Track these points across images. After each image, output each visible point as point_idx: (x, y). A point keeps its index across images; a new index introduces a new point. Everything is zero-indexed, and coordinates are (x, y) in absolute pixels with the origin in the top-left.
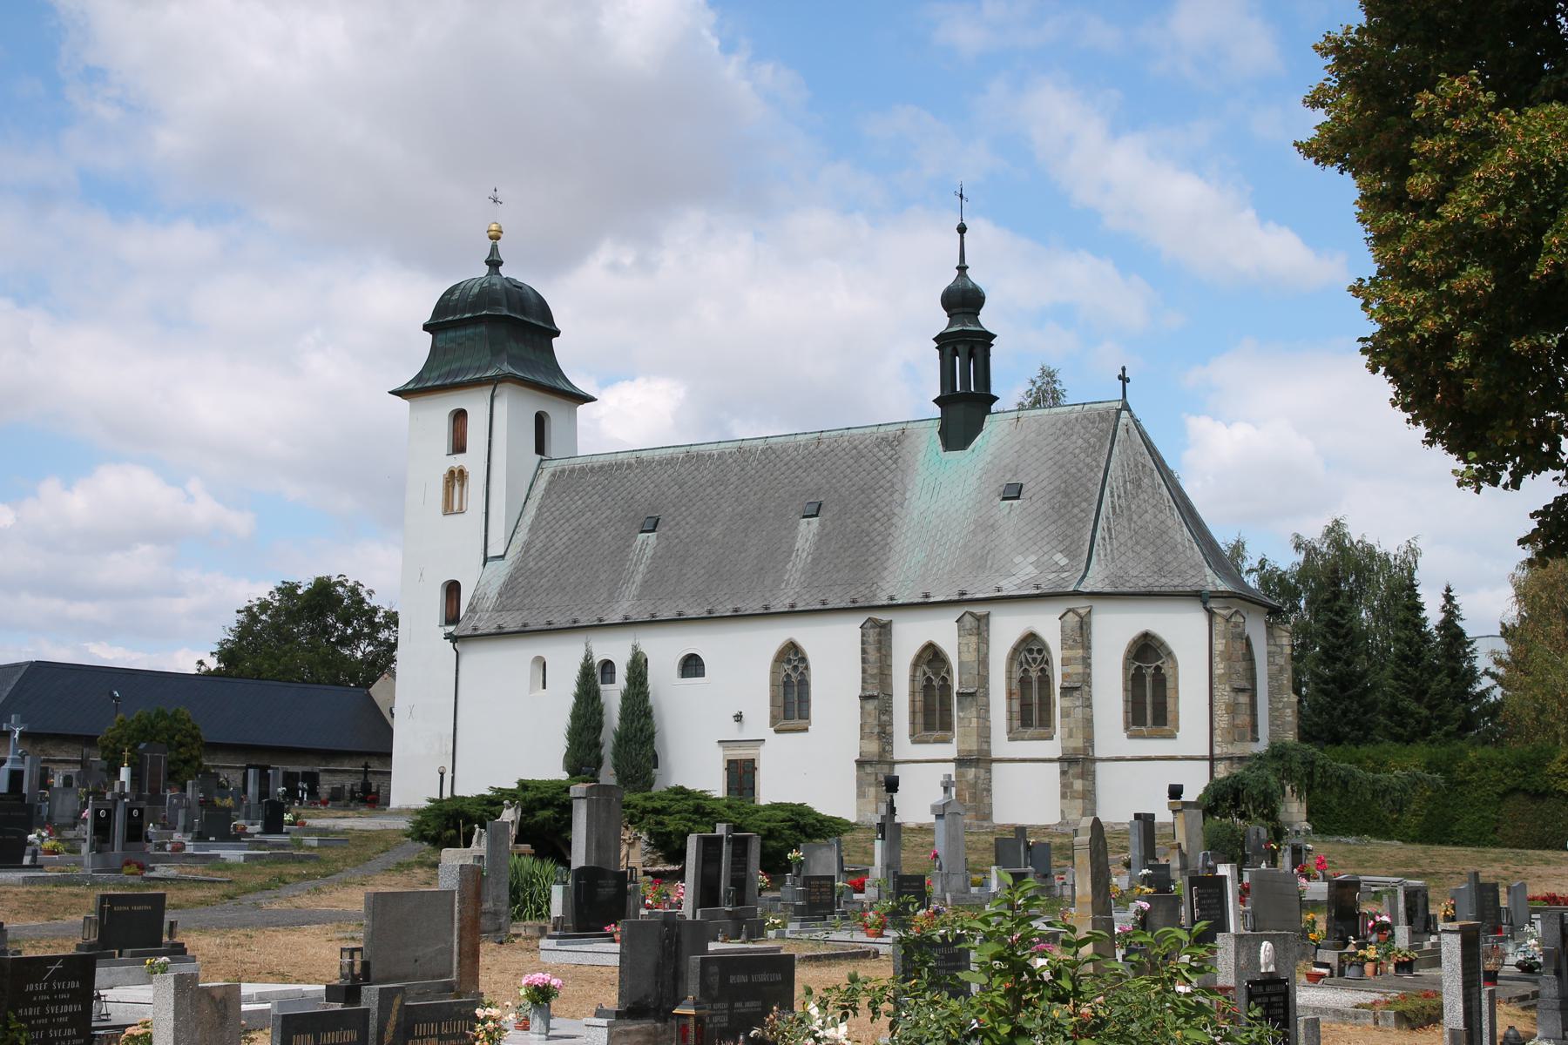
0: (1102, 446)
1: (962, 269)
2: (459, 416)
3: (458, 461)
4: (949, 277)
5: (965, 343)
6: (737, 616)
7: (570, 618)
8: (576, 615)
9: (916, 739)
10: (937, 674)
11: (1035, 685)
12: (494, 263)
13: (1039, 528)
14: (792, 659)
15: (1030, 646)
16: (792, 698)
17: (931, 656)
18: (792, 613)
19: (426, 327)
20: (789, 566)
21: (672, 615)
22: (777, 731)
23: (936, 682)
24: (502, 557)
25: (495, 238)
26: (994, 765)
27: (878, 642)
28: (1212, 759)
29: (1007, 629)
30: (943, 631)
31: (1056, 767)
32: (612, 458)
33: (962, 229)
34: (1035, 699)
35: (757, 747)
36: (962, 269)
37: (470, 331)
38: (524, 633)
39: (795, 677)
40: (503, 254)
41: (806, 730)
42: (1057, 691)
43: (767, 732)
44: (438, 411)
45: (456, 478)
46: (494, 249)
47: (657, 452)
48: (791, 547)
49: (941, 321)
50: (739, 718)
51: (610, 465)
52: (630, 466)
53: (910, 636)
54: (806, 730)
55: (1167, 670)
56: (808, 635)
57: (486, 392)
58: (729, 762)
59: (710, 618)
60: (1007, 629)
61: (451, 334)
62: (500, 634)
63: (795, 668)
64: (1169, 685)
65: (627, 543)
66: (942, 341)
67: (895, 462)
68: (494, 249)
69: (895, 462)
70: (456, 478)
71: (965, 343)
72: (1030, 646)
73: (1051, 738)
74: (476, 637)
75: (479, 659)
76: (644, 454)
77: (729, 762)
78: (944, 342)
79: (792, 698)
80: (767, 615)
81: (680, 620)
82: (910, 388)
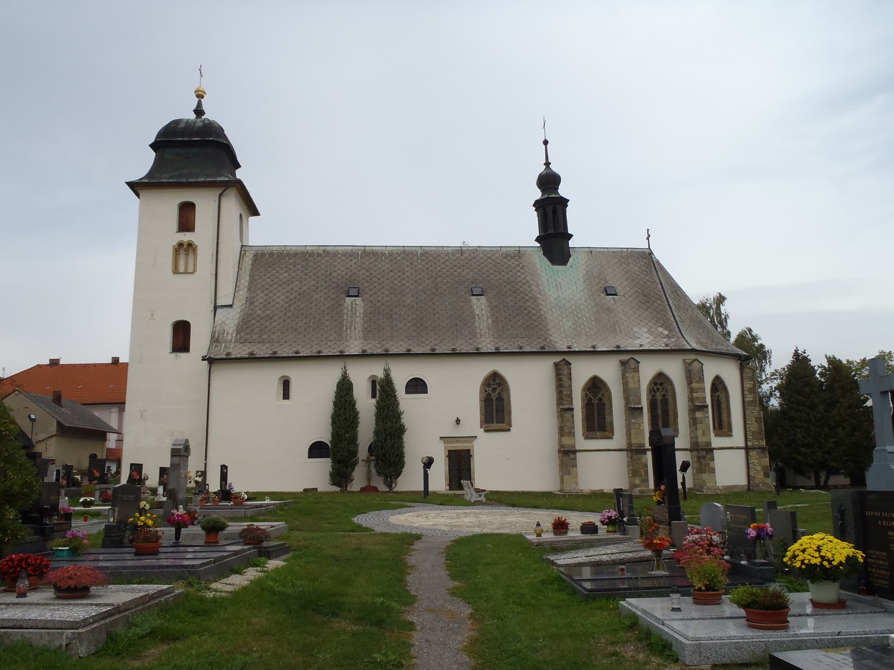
0: (651, 271)
1: (547, 164)
3: (186, 237)
5: (551, 209)
6: (454, 354)
7: (383, 348)
8: (388, 346)
10: (595, 396)
11: (659, 405)
12: (199, 112)
13: (639, 313)
16: (496, 408)
18: (497, 353)
19: (152, 146)
20: (477, 324)
22: (486, 431)
24: (231, 306)
27: (562, 375)
28: (747, 449)
31: (743, 452)
33: (546, 143)
34: (660, 412)
35: (471, 442)
36: (547, 164)
38: (274, 358)
39: (494, 396)
40: (205, 108)
41: (509, 430)
43: (479, 432)
44: (168, 204)
45: (185, 249)
46: (199, 104)
48: (472, 313)
49: (538, 194)
50: (458, 421)
51: (303, 253)
53: (582, 372)
54: (509, 430)
56: (509, 369)
57: (218, 192)
59: (433, 355)
60: (648, 369)
63: (494, 390)
64: (607, 406)
65: (338, 307)
66: (538, 205)
67: (522, 268)
68: (199, 104)
70: (185, 249)
71: (551, 209)
74: (229, 360)
76: (328, 249)
78: (539, 205)
79: (496, 408)
80: (478, 354)
82: (524, 231)
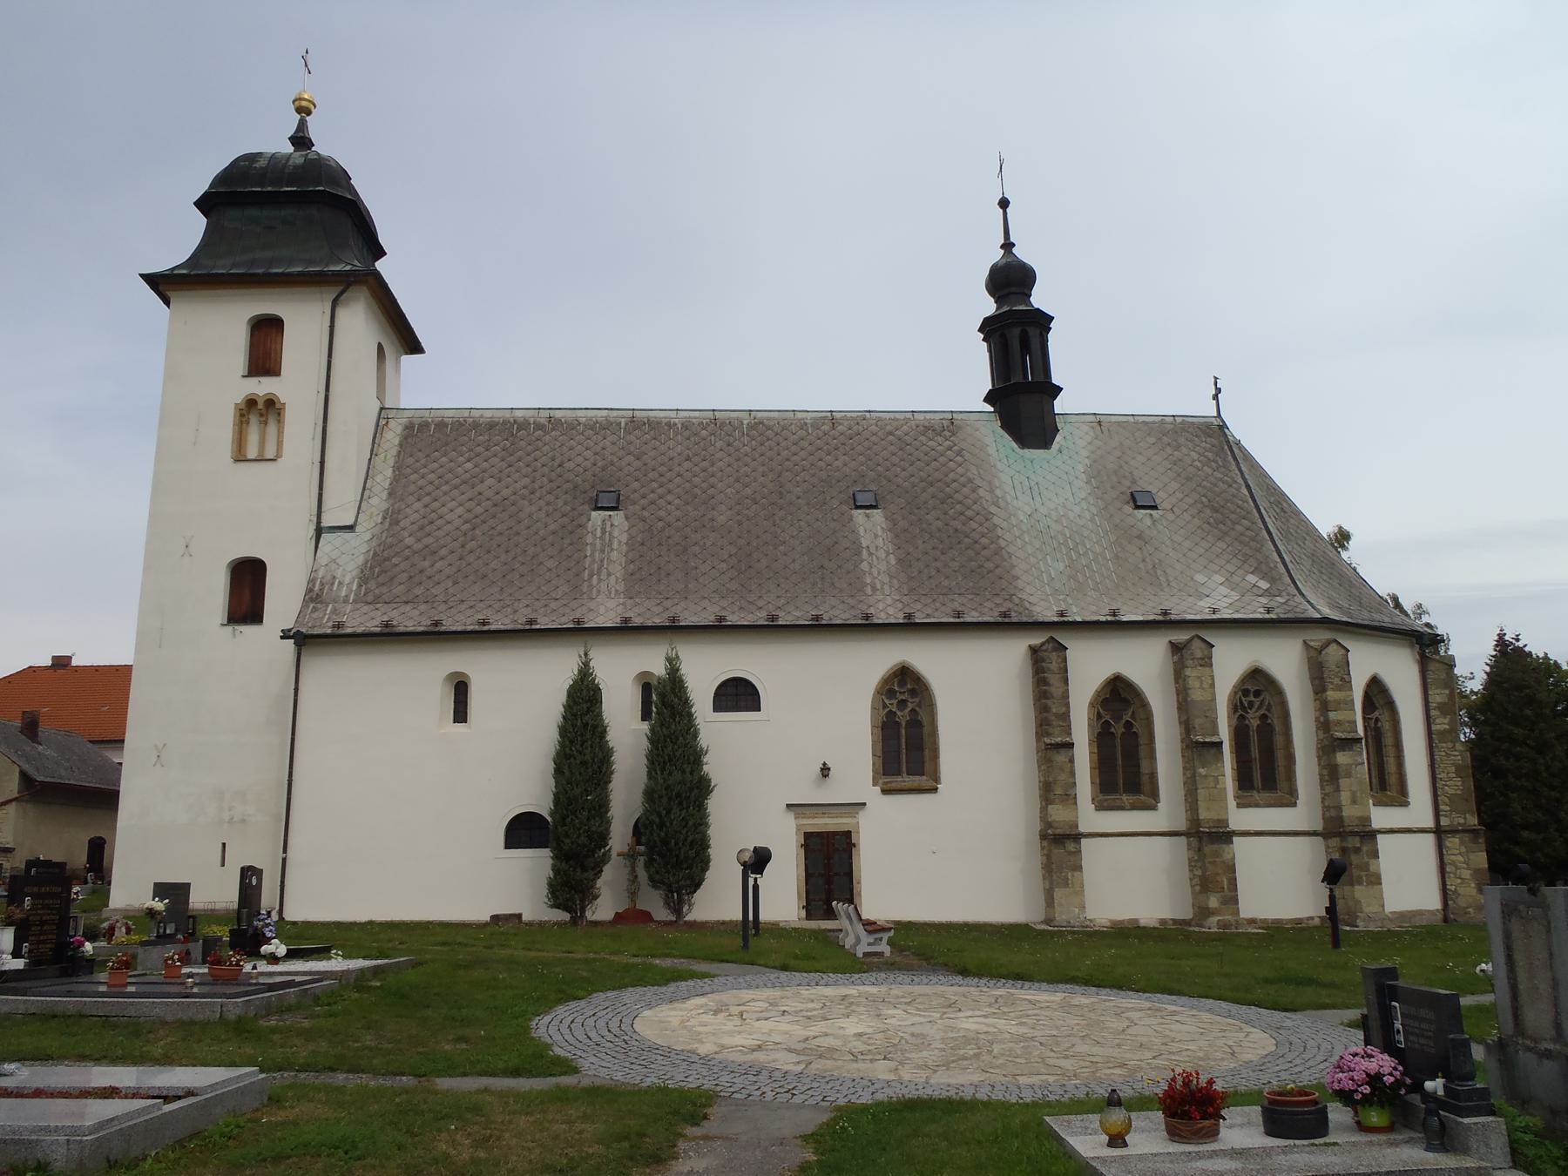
0: (1225, 460)
1: (1008, 246)
2: (266, 332)
3: (262, 387)
4: (997, 255)
5: (1016, 331)
6: (818, 628)
9: (1100, 807)
14: (584, 700)
15: (1257, 685)
16: (906, 742)
17: (1119, 696)
18: (909, 627)
21: (707, 618)
22: (885, 792)
23: (1118, 729)
24: (350, 528)
25: (304, 110)
26: (1083, 841)
29: (1231, 661)
30: (1144, 663)
31: (1429, 840)
32: (507, 414)
33: (1004, 203)
36: (1008, 246)
37: (287, 212)
38: (435, 636)
39: (903, 716)
41: (935, 790)
42: (1226, 748)
43: (870, 792)
44: (225, 323)
46: (302, 125)
47: (580, 413)
50: (825, 771)
52: (539, 426)
53: (1090, 666)
55: (1138, 727)
56: (936, 661)
58: (808, 836)
59: (771, 629)
60: (1231, 661)
61: (253, 212)
62: (388, 637)
63: (902, 703)
65: (575, 528)
67: (959, 453)
68: (302, 125)
69: (959, 453)
71: (1016, 331)
72: (1257, 685)
73: (1294, 805)
74: (339, 639)
75: (331, 676)
76: (558, 414)
77: (808, 836)
78: (990, 328)
79: (906, 742)
80: (868, 627)
81: (719, 629)
